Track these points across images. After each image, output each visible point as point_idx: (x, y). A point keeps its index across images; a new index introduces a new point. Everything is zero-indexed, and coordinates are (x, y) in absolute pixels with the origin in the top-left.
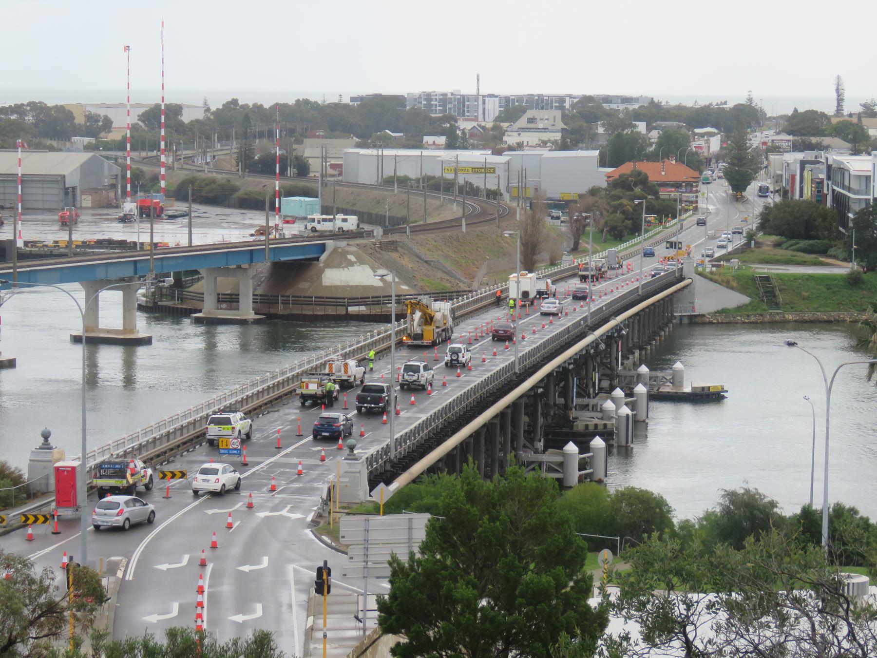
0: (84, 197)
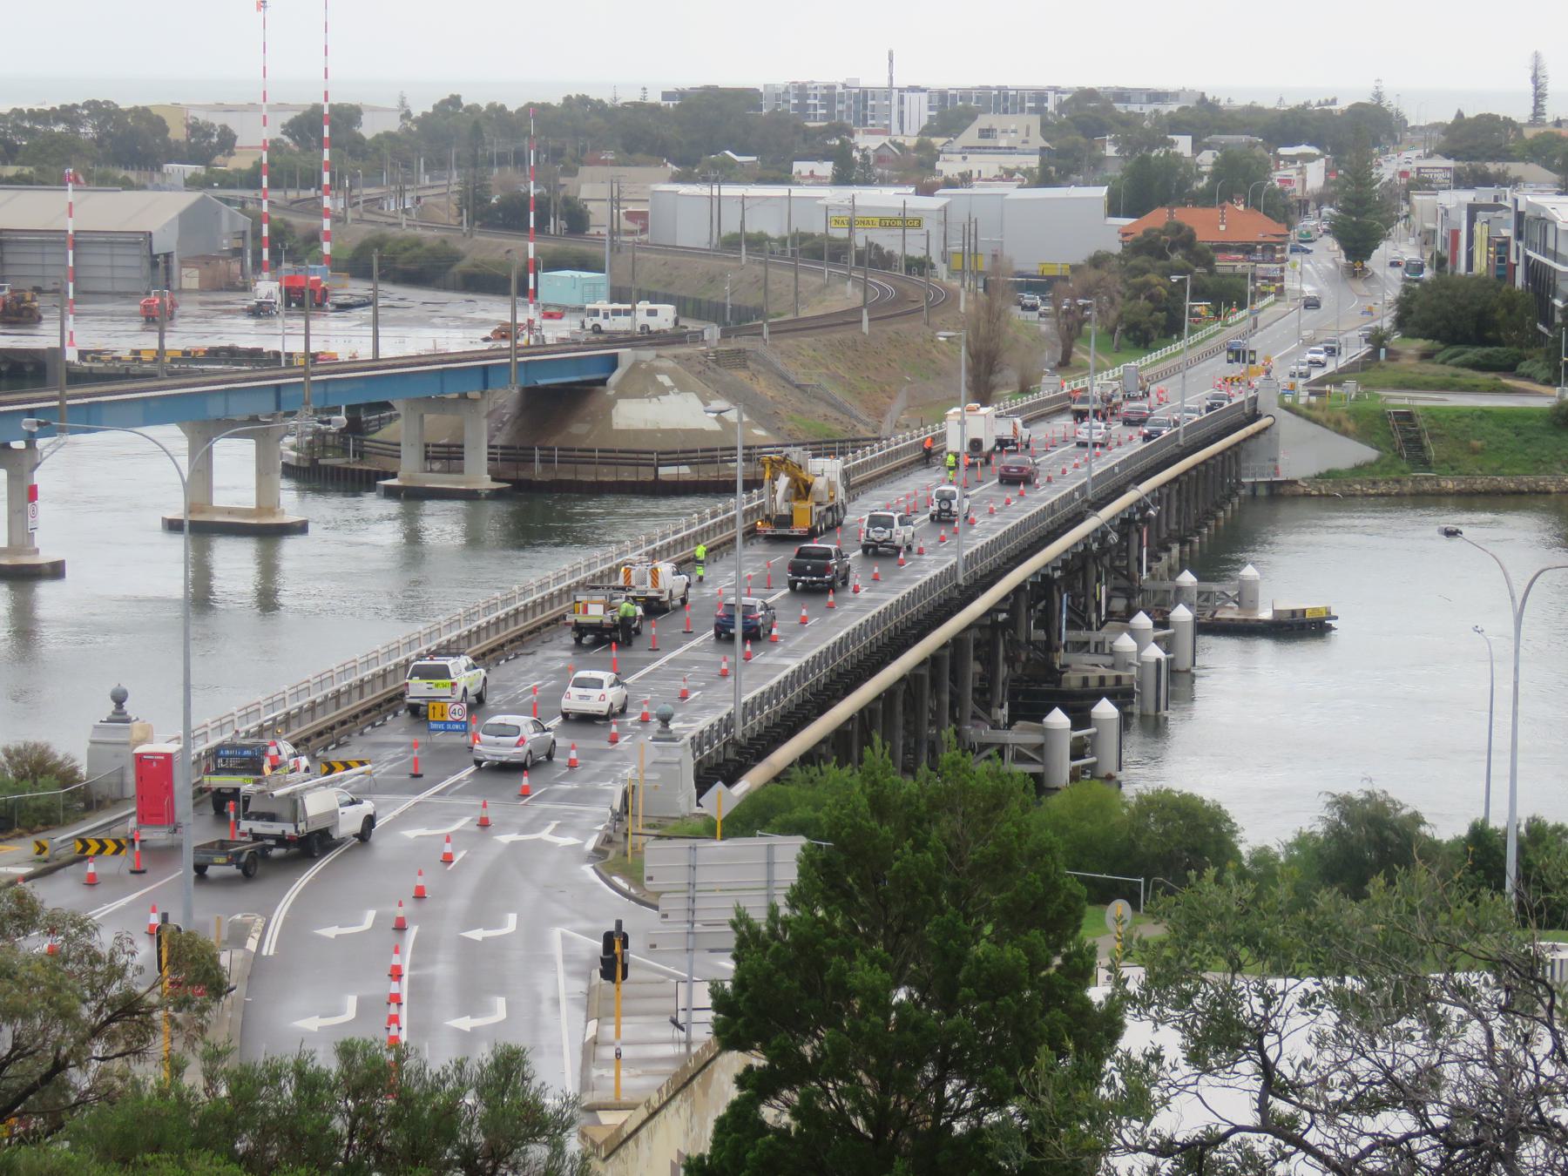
0: (185, 271)
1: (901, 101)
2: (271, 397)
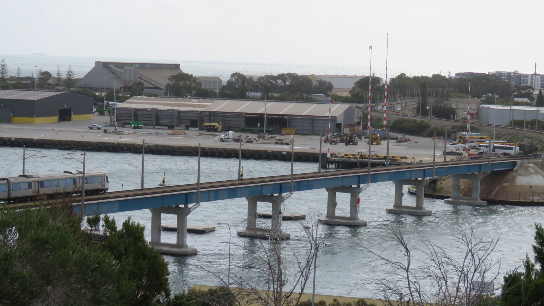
0: (345, 129)
1: (532, 79)
2: (423, 172)
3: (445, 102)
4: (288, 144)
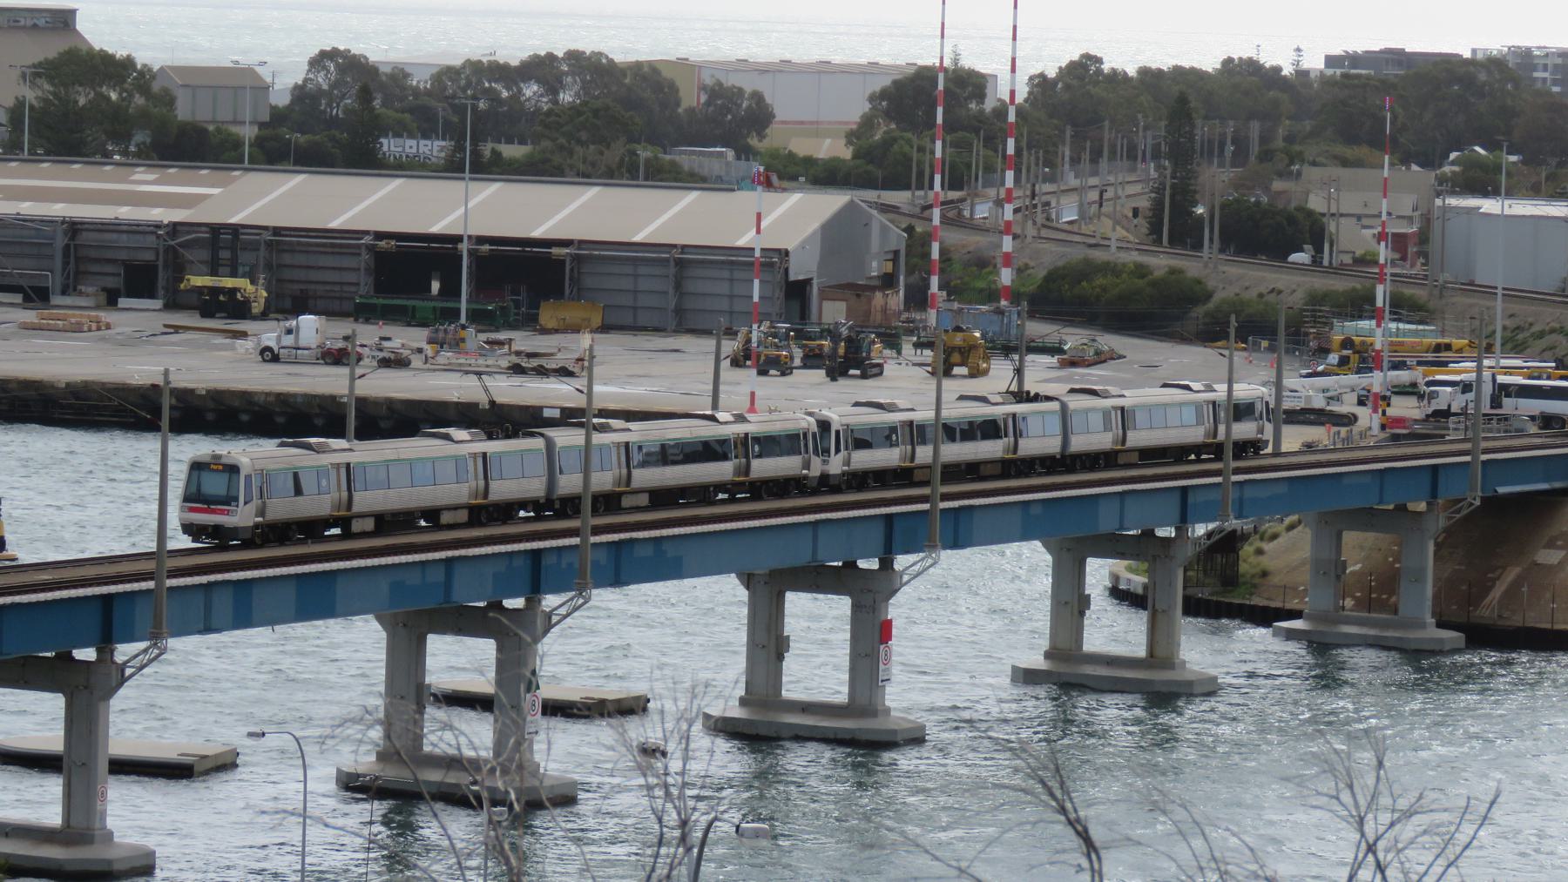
0: (827, 305)
2: (1175, 501)
3: (1278, 185)
4: (570, 374)
